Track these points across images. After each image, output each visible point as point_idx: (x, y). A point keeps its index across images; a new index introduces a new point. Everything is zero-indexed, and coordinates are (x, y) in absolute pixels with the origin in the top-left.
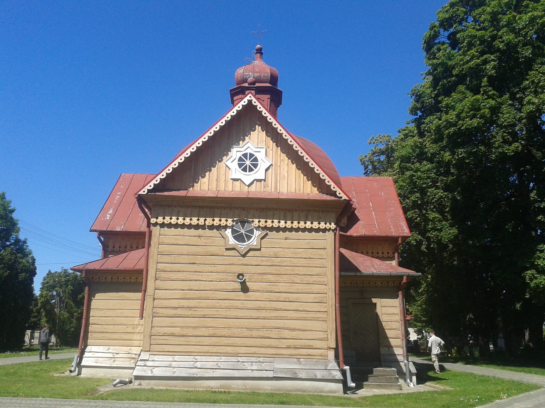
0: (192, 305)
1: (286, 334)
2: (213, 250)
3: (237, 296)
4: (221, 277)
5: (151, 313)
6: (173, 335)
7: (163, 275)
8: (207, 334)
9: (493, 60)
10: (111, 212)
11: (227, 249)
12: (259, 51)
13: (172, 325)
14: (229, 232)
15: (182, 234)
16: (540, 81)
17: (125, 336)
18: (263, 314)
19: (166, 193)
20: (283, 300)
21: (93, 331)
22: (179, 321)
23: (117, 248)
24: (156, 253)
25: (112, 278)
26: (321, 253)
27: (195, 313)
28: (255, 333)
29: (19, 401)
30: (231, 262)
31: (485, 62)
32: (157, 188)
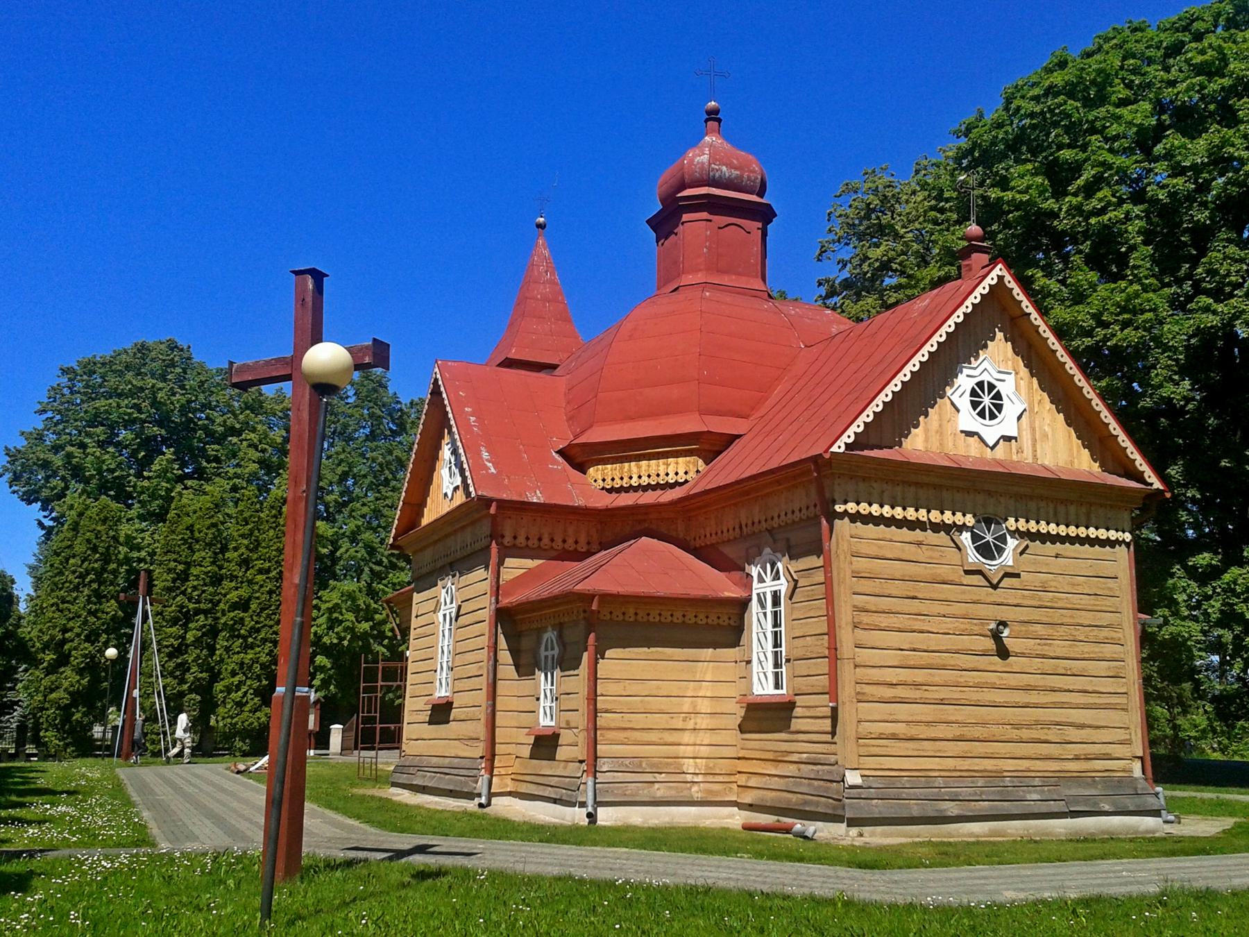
0: (919, 680)
1: (1073, 734)
2: (943, 571)
3: (991, 664)
4: (962, 626)
5: (853, 694)
6: (894, 737)
7: (866, 618)
8: (950, 736)
9: (1137, 216)
10: (485, 455)
11: (967, 572)
12: (713, 115)
13: (891, 718)
14: (966, 537)
15: (888, 537)
16: (1228, 274)
17: (668, 737)
18: (1033, 698)
19: (866, 453)
20: (1063, 672)
21: (605, 725)
22: (902, 711)
23: (521, 540)
24: (849, 574)
25: (636, 614)
26: (1110, 586)
27: (927, 695)
28: (1025, 734)
29: (877, 877)
30: (975, 598)
31: (1128, 218)
32: (860, 442)
